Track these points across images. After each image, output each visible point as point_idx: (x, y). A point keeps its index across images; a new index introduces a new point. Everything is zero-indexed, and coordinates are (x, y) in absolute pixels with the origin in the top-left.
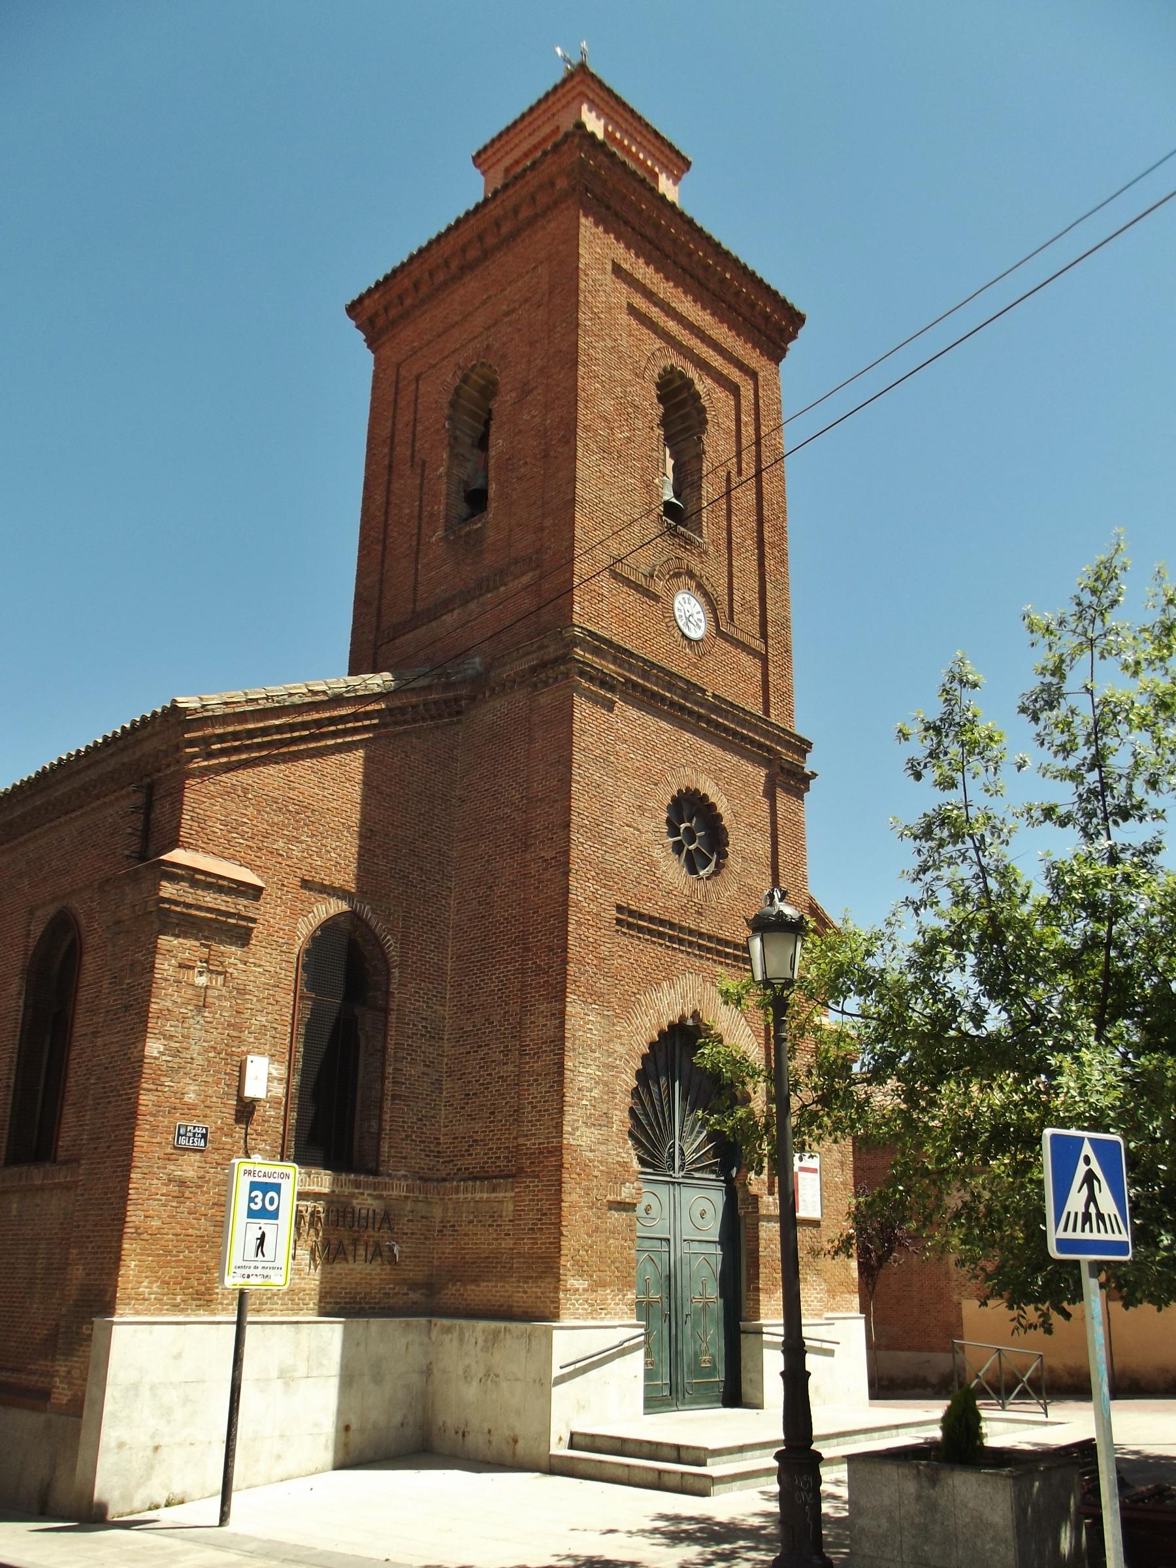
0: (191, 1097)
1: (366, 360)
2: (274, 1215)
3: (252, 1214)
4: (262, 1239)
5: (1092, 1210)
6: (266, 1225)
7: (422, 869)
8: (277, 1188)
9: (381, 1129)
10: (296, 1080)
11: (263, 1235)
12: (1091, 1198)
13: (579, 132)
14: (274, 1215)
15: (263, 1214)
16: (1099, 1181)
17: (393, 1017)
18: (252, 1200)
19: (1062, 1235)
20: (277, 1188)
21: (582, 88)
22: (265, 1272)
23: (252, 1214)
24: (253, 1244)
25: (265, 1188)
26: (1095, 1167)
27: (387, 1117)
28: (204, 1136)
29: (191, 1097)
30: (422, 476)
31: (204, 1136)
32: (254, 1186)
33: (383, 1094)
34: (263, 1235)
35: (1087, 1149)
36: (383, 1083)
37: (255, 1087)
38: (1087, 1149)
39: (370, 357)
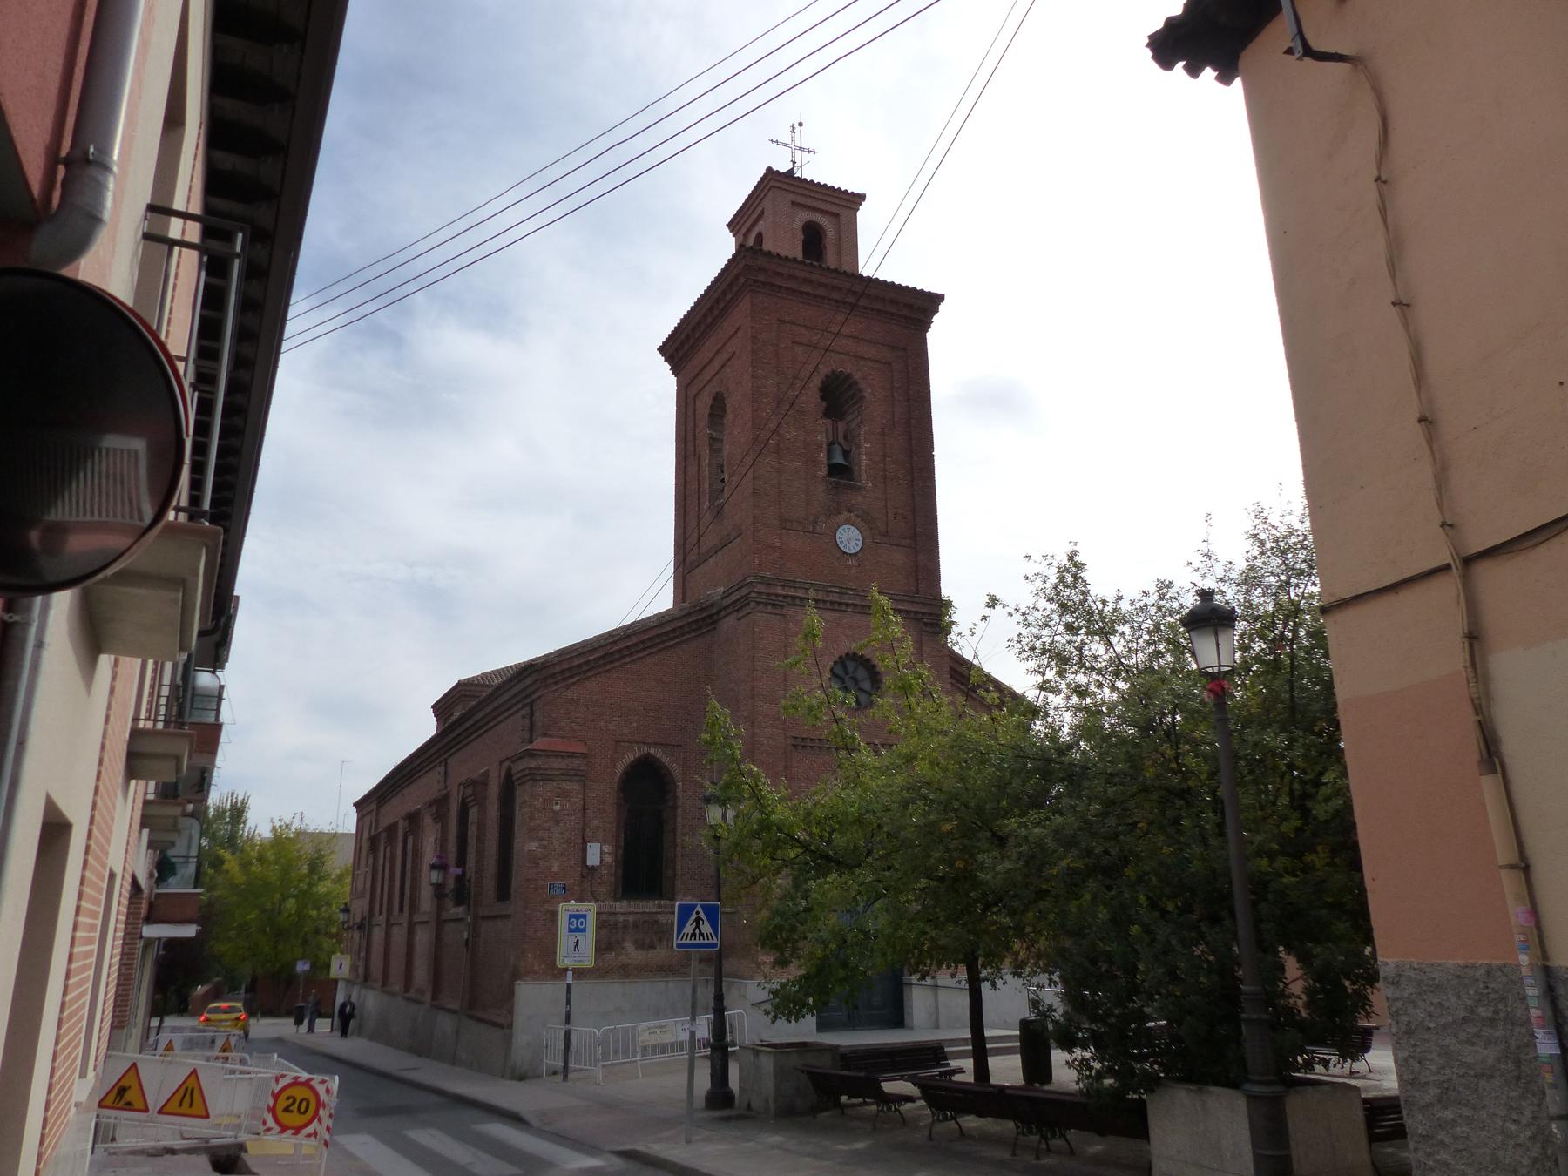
0: (555, 869)
1: (670, 383)
2: (584, 930)
3: (571, 930)
4: (577, 942)
5: (697, 931)
6: (580, 936)
7: (693, 722)
8: (584, 917)
9: (675, 875)
10: (621, 852)
11: (578, 940)
12: (698, 926)
13: (743, 249)
14: (584, 930)
15: (577, 930)
16: (703, 921)
17: (679, 811)
18: (570, 923)
19: (679, 941)
20: (584, 917)
21: (772, 183)
22: (579, 959)
23: (571, 930)
24: (573, 945)
25: (577, 917)
26: (702, 915)
27: (679, 867)
28: (564, 888)
29: (555, 869)
30: (699, 465)
31: (564, 888)
32: (571, 916)
33: (676, 855)
34: (578, 940)
35: (699, 909)
36: (675, 849)
37: (593, 858)
38: (699, 909)
39: (674, 379)
